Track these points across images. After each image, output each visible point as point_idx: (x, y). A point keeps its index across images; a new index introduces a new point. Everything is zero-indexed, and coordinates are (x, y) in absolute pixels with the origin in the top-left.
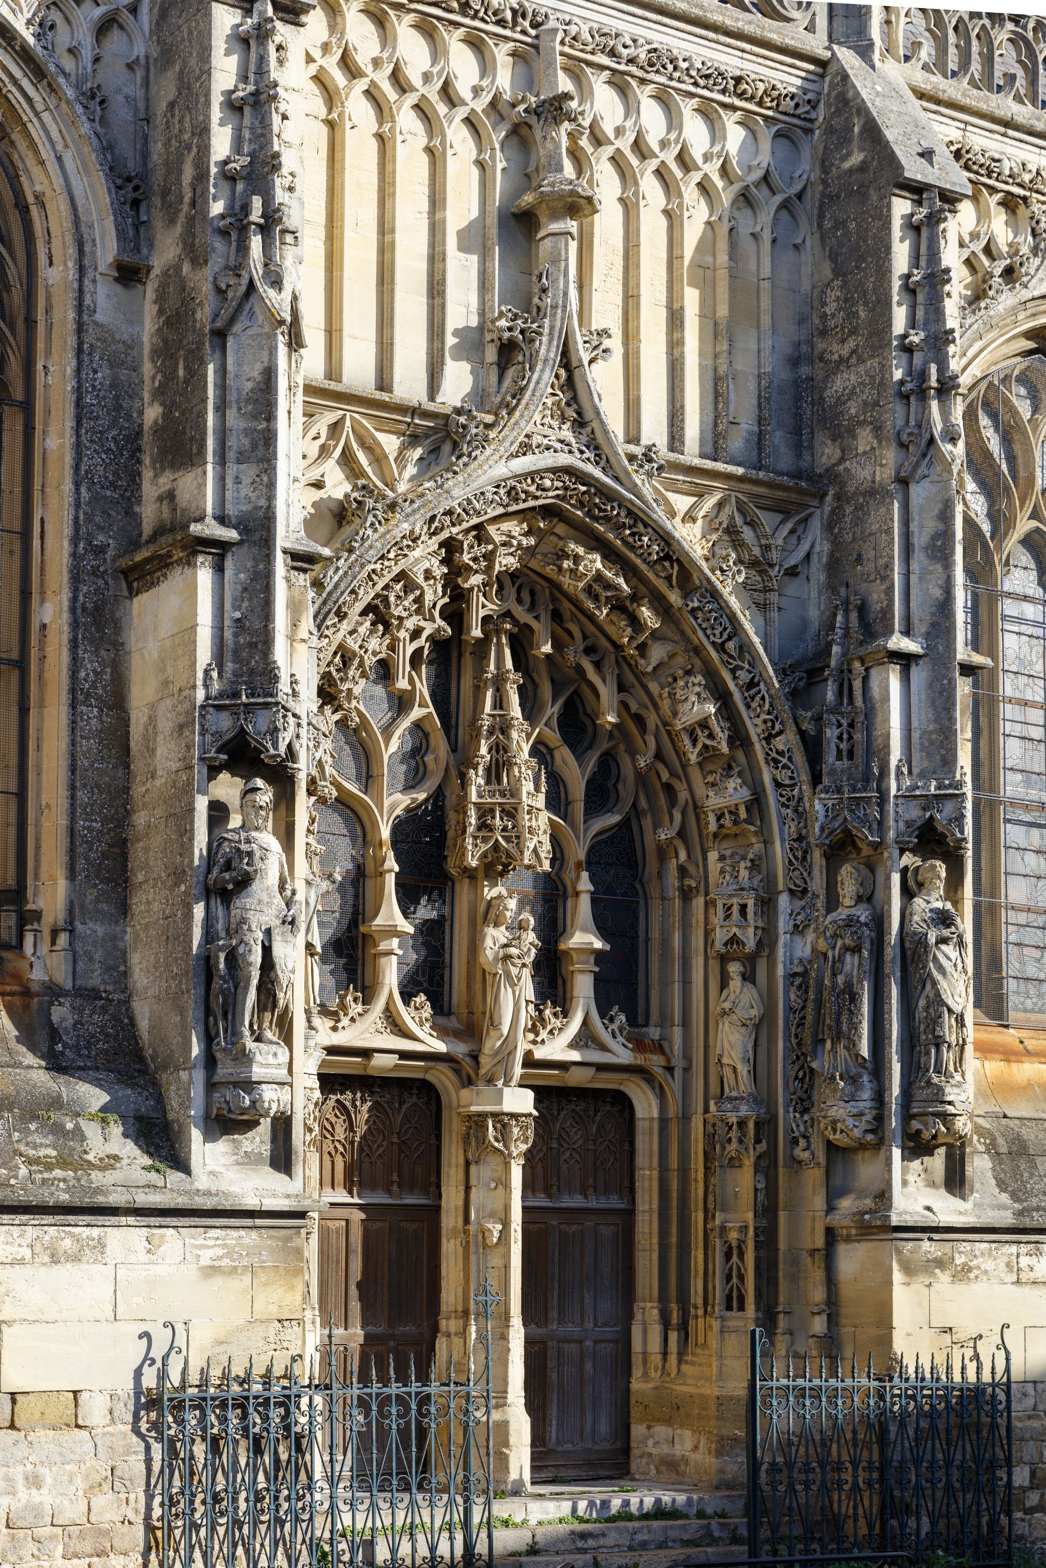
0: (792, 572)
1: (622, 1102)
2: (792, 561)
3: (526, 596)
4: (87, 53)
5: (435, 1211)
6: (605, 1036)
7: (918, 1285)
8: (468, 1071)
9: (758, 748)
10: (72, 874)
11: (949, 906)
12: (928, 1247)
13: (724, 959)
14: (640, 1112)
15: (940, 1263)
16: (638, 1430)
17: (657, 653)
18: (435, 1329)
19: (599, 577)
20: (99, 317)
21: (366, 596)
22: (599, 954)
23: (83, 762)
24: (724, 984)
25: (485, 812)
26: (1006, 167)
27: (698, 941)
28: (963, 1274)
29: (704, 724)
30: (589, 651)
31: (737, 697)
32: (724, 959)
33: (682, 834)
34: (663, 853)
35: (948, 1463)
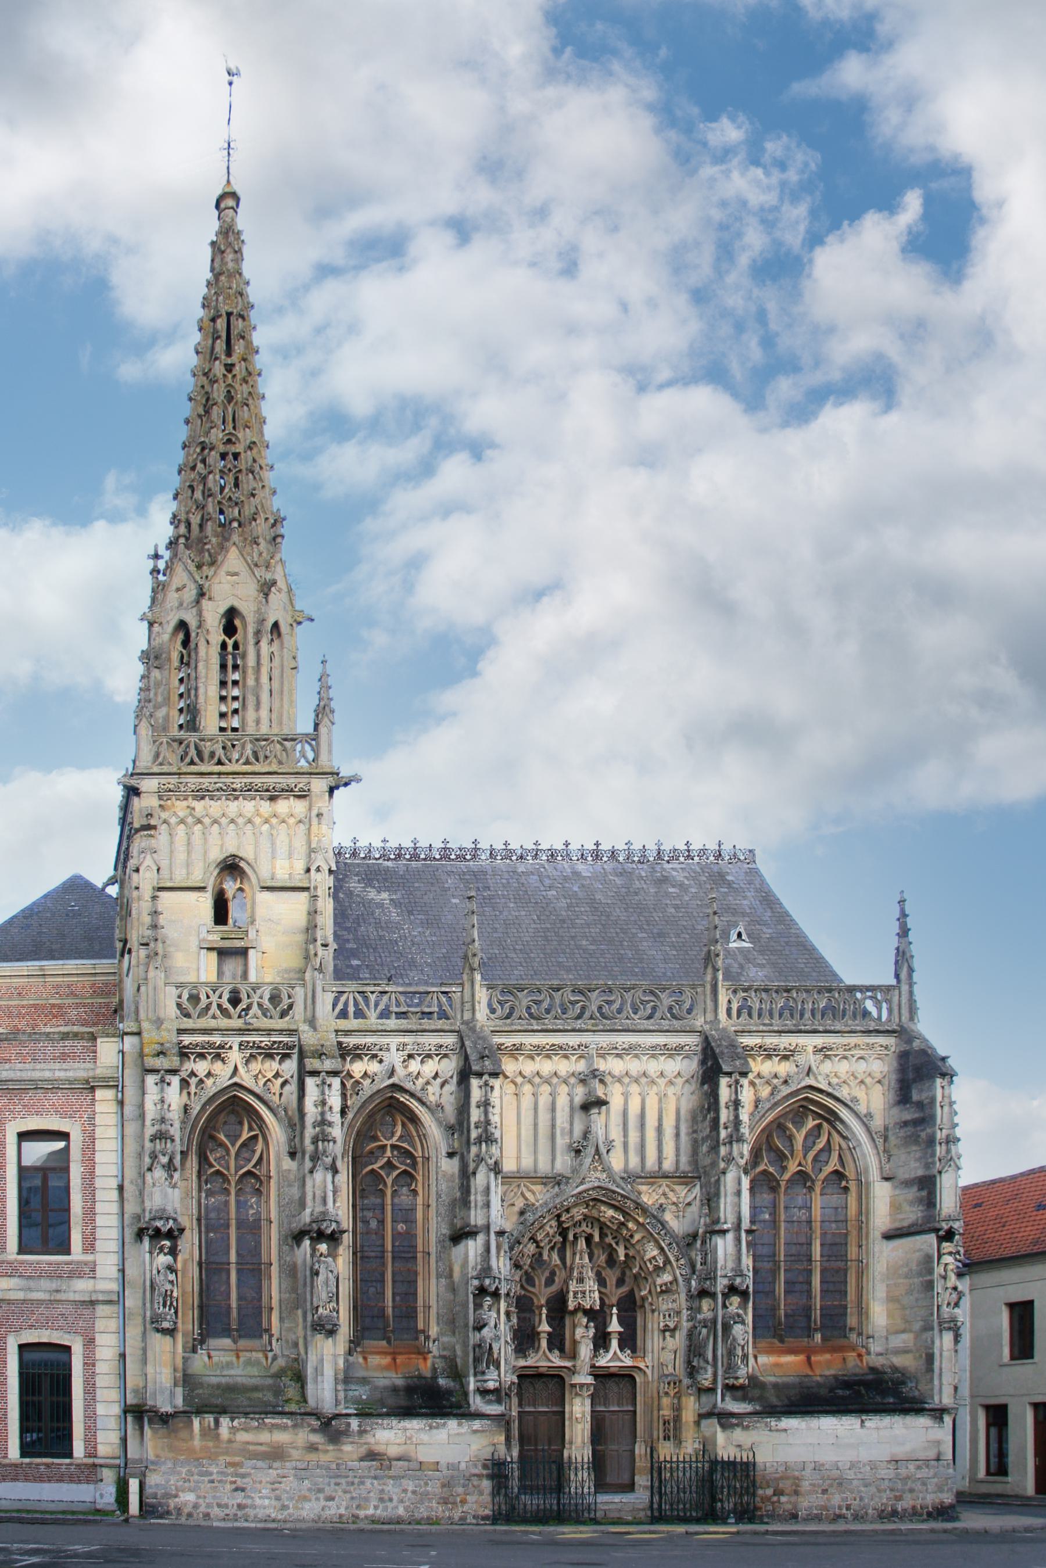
0: (689, 1204)
1: (632, 1378)
2: (688, 1200)
3: (590, 1225)
4: (438, 1095)
5: (563, 1412)
6: (622, 1357)
7: (728, 1432)
8: (573, 1371)
9: (674, 1264)
10: (438, 1324)
11: (741, 1312)
12: (734, 1421)
13: (664, 1331)
14: (638, 1380)
15: (737, 1425)
16: (637, 1478)
17: (637, 1237)
18: (564, 1447)
19: (613, 1217)
20: (443, 1169)
21: (528, 1235)
22: (620, 1333)
23: (441, 1294)
24: (664, 1339)
25: (575, 1293)
26: (782, 1047)
27: (656, 1326)
28: (747, 1428)
29: (654, 1258)
30: (613, 1238)
31: (666, 1248)
32: (664, 1331)
33: (650, 1292)
34: (643, 1299)
35: (741, 1487)
